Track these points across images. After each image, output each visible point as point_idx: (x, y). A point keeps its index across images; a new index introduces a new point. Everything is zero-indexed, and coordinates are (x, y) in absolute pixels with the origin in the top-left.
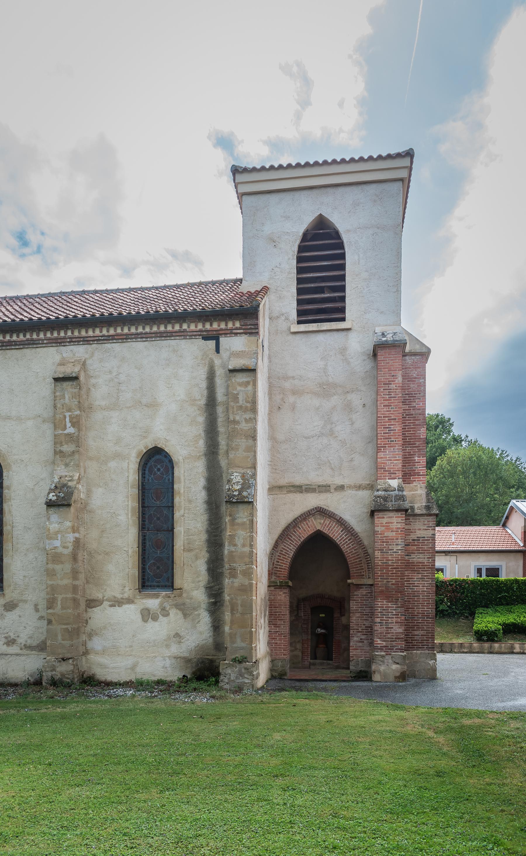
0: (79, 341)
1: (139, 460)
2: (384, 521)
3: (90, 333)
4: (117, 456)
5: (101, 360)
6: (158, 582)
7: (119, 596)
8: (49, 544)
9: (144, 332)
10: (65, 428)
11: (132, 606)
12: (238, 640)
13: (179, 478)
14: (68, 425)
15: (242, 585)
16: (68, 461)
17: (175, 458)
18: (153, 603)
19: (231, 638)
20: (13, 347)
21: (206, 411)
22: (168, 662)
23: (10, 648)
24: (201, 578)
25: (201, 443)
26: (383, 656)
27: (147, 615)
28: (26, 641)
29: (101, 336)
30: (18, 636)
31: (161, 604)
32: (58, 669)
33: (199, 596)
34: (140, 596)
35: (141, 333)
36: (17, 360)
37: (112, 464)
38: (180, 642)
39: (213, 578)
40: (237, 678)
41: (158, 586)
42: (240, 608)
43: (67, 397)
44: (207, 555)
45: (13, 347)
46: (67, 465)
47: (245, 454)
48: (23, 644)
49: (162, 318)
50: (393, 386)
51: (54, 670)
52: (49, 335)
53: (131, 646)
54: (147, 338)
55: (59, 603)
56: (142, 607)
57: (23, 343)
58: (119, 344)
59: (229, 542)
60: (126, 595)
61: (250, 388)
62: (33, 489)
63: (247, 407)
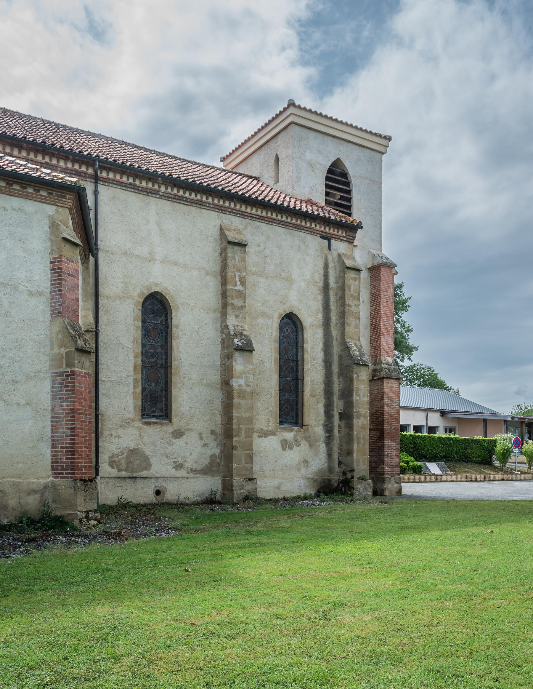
0: (237, 214)
1: (279, 321)
2: (389, 385)
3: (249, 210)
4: (264, 314)
5: (252, 234)
6: (287, 419)
7: (265, 429)
8: (236, 382)
9: (286, 221)
10: (235, 285)
11: (274, 438)
12: (361, 464)
13: (307, 340)
14: (238, 283)
15: (363, 425)
16: (238, 313)
17: (304, 324)
18: (289, 435)
19: (357, 462)
20: (182, 202)
21: (323, 293)
22: (302, 482)
23: (178, 472)
24: (320, 418)
25: (320, 315)
26: (390, 478)
27: (286, 445)
28: (192, 466)
29: (255, 215)
30: (185, 461)
31: (295, 436)
32: (246, 488)
33: (319, 431)
34: (280, 429)
35: (284, 222)
36: (184, 214)
37: (260, 321)
38: (307, 467)
39: (327, 418)
40: (364, 491)
41: (286, 422)
42: (362, 441)
43: (237, 259)
44: (324, 401)
45: (182, 202)
46: (237, 316)
47: (355, 330)
48: (189, 469)
49: (301, 215)
50: (388, 294)
51: (243, 489)
52: (216, 201)
53: (274, 470)
54: (286, 226)
55: (243, 432)
56: (282, 438)
57: (192, 201)
58: (265, 224)
59: (356, 393)
60: (270, 428)
61: (357, 283)
62: (197, 332)
63: (355, 296)
